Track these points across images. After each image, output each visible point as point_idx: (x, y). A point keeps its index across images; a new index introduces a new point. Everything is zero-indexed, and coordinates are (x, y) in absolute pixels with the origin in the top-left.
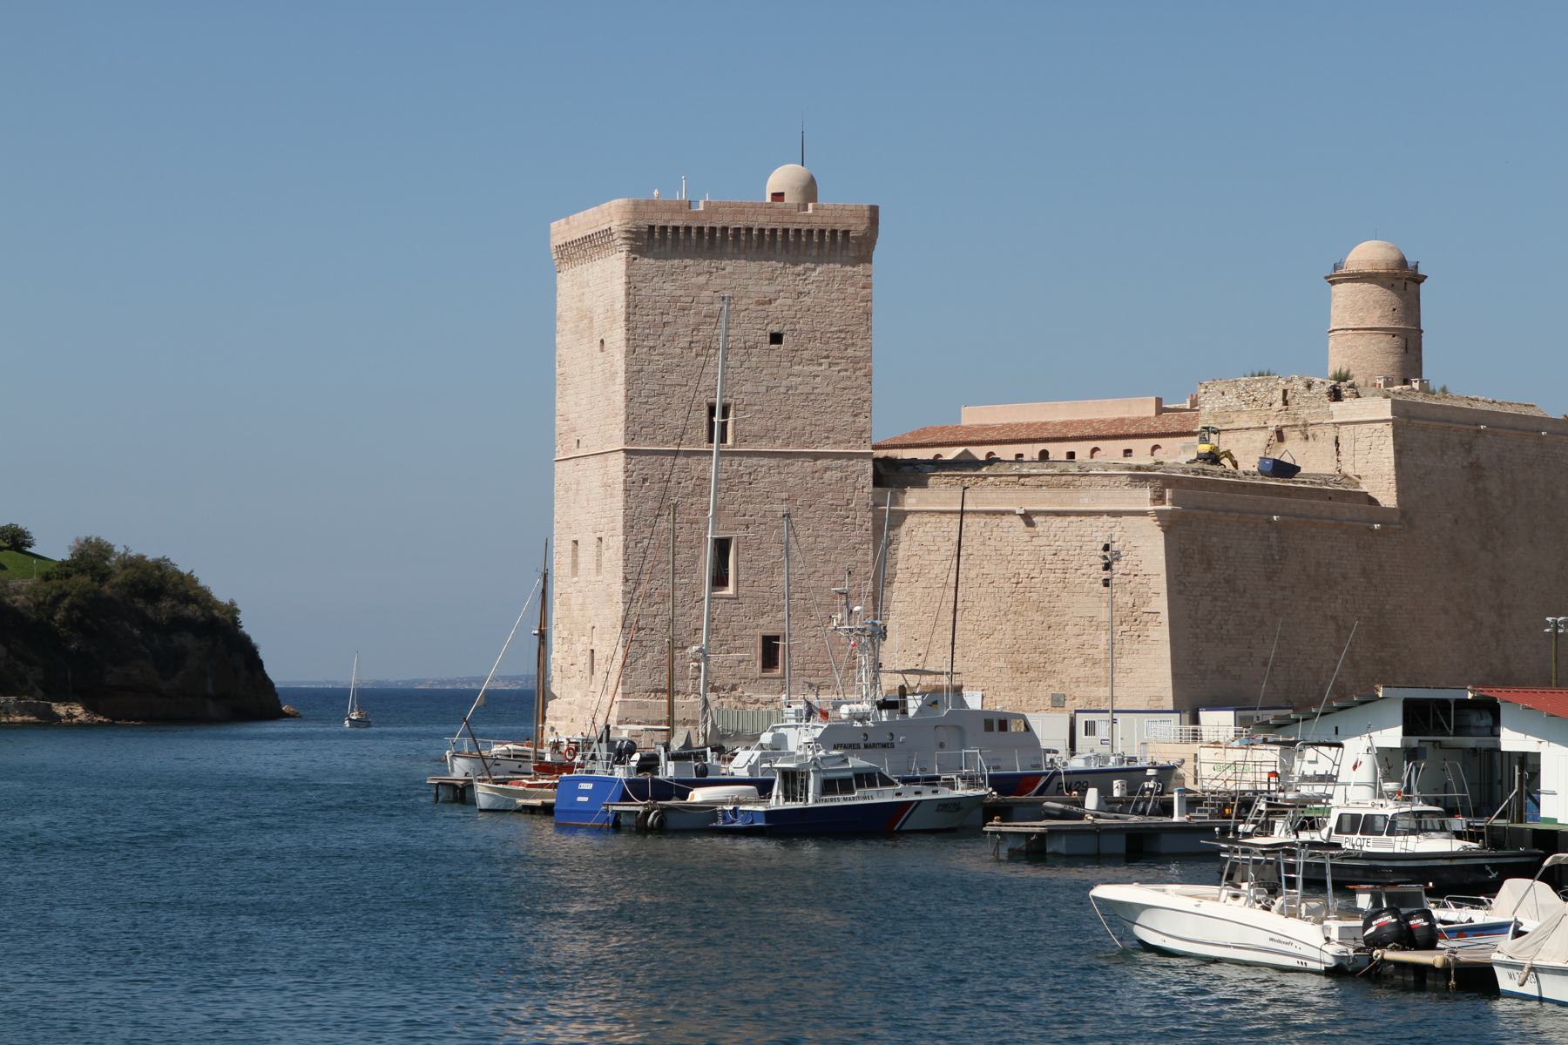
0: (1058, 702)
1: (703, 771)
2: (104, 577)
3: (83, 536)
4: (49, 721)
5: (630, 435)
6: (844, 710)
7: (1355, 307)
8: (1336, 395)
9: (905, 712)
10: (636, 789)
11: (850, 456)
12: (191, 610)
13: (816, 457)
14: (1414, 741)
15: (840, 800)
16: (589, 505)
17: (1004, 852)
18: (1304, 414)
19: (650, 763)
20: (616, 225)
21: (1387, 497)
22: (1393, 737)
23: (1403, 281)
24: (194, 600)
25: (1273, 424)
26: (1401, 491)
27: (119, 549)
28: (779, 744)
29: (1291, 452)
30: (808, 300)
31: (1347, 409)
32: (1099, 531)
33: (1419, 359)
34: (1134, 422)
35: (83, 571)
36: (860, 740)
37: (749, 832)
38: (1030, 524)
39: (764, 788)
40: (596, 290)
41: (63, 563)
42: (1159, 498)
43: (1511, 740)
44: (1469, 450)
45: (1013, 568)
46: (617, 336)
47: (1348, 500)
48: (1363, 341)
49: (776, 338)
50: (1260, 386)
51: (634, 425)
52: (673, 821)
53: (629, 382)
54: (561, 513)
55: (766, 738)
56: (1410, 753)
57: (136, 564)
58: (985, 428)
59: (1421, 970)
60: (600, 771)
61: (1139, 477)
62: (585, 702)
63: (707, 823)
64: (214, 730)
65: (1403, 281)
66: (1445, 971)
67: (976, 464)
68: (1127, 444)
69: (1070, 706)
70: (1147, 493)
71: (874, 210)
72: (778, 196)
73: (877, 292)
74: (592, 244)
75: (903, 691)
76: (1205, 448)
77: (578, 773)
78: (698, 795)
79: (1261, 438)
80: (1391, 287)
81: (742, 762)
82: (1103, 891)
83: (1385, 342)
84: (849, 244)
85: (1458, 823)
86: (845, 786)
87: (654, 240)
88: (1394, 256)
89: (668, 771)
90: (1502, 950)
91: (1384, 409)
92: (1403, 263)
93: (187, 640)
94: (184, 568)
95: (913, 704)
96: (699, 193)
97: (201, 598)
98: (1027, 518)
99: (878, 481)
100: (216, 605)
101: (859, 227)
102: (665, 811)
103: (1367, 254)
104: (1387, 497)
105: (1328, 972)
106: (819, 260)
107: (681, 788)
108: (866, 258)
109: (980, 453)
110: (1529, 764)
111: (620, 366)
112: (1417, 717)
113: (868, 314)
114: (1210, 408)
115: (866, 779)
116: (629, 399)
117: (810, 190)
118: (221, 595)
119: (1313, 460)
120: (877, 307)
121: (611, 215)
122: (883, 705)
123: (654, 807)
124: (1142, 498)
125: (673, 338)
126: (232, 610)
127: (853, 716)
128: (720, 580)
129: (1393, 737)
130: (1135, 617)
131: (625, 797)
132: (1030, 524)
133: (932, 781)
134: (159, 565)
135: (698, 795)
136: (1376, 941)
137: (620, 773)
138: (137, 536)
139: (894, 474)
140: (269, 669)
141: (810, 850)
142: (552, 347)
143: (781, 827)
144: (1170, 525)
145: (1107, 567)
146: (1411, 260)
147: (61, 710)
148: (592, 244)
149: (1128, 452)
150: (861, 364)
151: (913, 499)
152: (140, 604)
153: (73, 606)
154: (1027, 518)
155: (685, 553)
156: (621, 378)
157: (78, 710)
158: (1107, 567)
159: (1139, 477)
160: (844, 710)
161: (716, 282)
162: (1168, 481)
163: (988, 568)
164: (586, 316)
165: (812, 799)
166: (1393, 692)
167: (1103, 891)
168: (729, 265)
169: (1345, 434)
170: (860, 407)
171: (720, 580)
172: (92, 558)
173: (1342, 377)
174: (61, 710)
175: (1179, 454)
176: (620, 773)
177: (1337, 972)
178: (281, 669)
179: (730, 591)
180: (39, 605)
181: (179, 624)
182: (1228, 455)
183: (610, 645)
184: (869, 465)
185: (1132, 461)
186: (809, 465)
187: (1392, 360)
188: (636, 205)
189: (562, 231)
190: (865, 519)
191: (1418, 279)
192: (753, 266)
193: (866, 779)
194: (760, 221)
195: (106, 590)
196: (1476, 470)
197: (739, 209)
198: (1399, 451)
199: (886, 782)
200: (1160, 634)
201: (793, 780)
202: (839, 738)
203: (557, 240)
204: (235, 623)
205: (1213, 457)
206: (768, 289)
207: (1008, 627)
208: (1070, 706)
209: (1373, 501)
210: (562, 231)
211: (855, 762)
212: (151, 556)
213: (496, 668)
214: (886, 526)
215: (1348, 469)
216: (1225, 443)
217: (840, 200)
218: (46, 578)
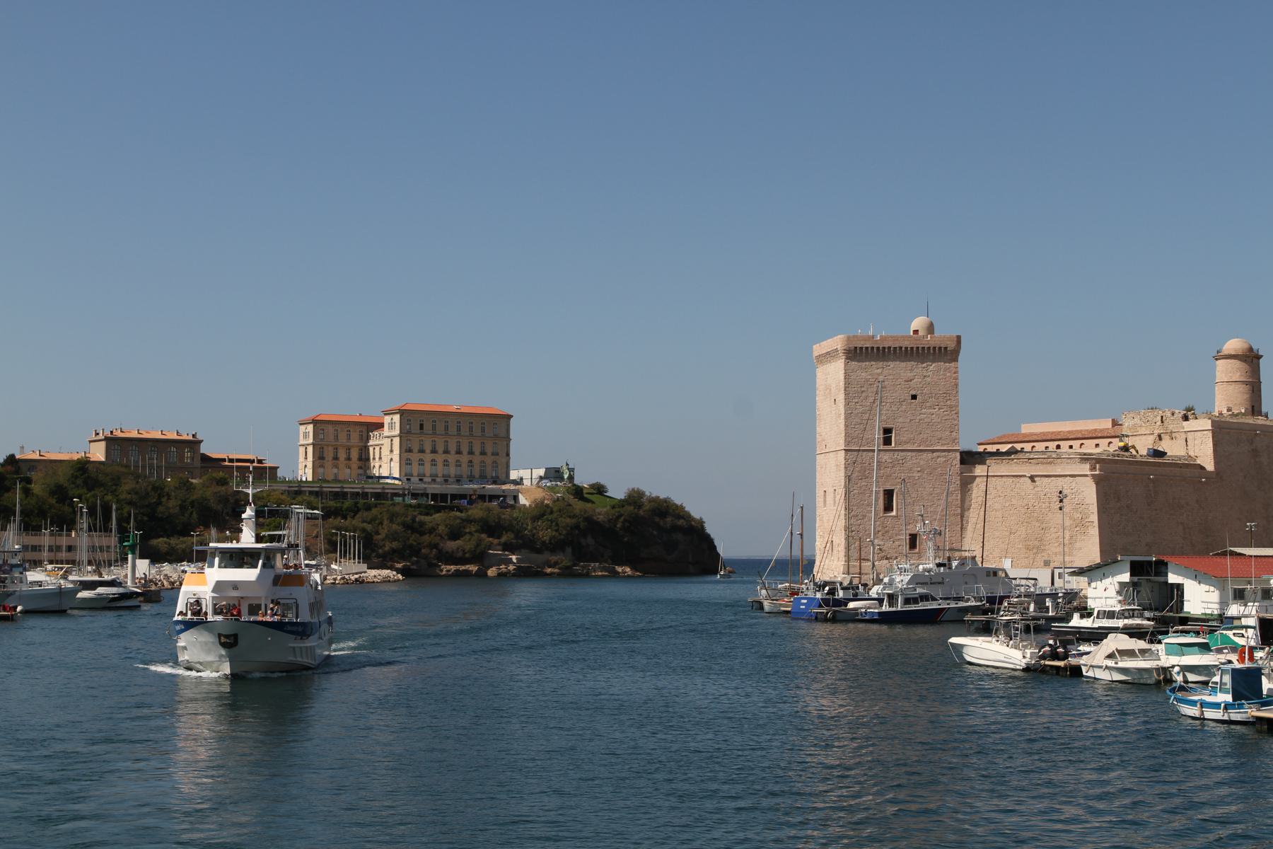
0: (1047, 563)
1: (856, 595)
2: (640, 507)
3: (631, 487)
4: (614, 575)
5: (847, 442)
6: (921, 567)
7: (1227, 371)
8: (1186, 418)
9: (950, 568)
10: (826, 602)
11: (949, 451)
12: (681, 522)
13: (933, 451)
14: (1136, 579)
15: (913, 607)
16: (830, 473)
17: (972, 628)
18: (1171, 427)
19: (832, 592)
20: (839, 347)
21: (1210, 467)
22: (1126, 577)
23: (1251, 358)
24: (683, 518)
25: (1157, 432)
26: (1216, 463)
27: (647, 494)
28: (891, 582)
29: (1165, 446)
30: (928, 379)
31: (1191, 425)
32: (1052, 486)
33: (1260, 396)
34: (1101, 430)
35: (630, 504)
36: (928, 580)
37: (872, 621)
38: (1033, 481)
39: (881, 601)
40: (832, 375)
41: (621, 500)
42: (1093, 468)
43: (1173, 578)
44: (1252, 443)
45: (1026, 502)
46: (841, 398)
47: (1190, 469)
48: (1232, 387)
49: (914, 397)
50: (1150, 415)
51: (849, 438)
52: (839, 616)
53: (846, 418)
54: (819, 478)
55: (886, 580)
56: (1134, 585)
57: (655, 500)
58: (1032, 434)
59: (1058, 668)
60: (810, 594)
61: (1085, 458)
62: (831, 566)
63: (854, 617)
64: (695, 579)
65: (1251, 358)
66: (1065, 668)
67: (1016, 452)
68: (1097, 441)
69: (1052, 565)
70: (1088, 466)
71: (959, 338)
72: (916, 332)
73: (960, 375)
74: (829, 356)
75: (949, 559)
76: (1122, 444)
77: (801, 595)
78: (851, 605)
79: (1151, 439)
80: (1245, 361)
81: (875, 591)
82: (954, 640)
83: (1242, 388)
84: (947, 353)
85: (1147, 614)
86: (915, 601)
87: (857, 353)
88: (1246, 346)
89: (841, 594)
90: (1082, 661)
91: (1208, 424)
92: (1251, 349)
93: (678, 537)
94: (678, 502)
95: (955, 564)
96: (877, 331)
97: (686, 516)
98: (1032, 478)
99: (962, 462)
100: (694, 519)
101: (951, 346)
102: (835, 612)
103: (1233, 345)
104: (1210, 467)
105: (1024, 670)
106: (933, 361)
107: (844, 602)
108: (956, 360)
109: (1018, 446)
110: (1180, 587)
111: (842, 411)
112: (1136, 569)
113: (957, 385)
114: (1128, 423)
115: (925, 598)
116: (846, 426)
117: (930, 328)
118: (696, 514)
119: (1174, 449)
120: (960, 382)
121: (837, 342)
122: (939, 565)
123: (833, 608)
124: (1085, 468)
125: (866, 397)
126: (701, 522)
127: (925, 570)
128: (888, 508)
129: (1126, 577)
130: (1082, 524)
131: (820, 606)
132: (1033, 481)
133: (959, 599)
134: (666, 501)
135: (851, 605)
136: (1043, 657)
137: (819, 595)
138: (656, 489)
139: (970, 459)
140: (720, 550)
141: (899, 630)
142: (815, 402)
143: (885, 618)
144: (1098, 481)
145: (1061, 501)
146: (1255, 348)
147: (619, 569)
148: (829, 356)
149: (1097, 445)
150: (954, 408)
151: (979, 470)
152: (657, 519)
153: (625, 520)
154: (1032, 478)
155: (875, 498)
156: (843, 417)
157: (628, 569)
158: (1061, 501)
159: (1085, 458)
160: (921, 567)
161: (886, 372)
162: (1099, 461)
163: (1014, 502)
164: (828, 388)
165: (899, 607)
166: (1125, 558)
167: (954, 640)
168: (892, 364)
169: (1190, 436)
170: (953, 428)
171: (888, 508)
172: (635, 498)
173: (1189, 410)
174: (619, 569)
175: (1108, 448)
176: (819, 595)
177: (1027, 669)
178: (725, 549)
179: (894, 513)
180: (610, 520)
181: (675, 528)
182: (1133, 447)
183: (840, 539)
184: (958, 455)
185: (1084, 450)
186: (930, 455)
187: (1246, 396)
188: (849, 338)
189: (818, 349)
190: (956, 480)
191: (1259, 357)
192: (903, 364)
193: (925, 598)
194: (906, 344)
195: (641, 512)
196: (1255, 453)
197: (895, 339)
198: (1215, 445)
199: (934, 599)
200: (1094, 531)
201: (892, 598)
202: (917, 580)
203: (816, 354)
204: (703, 528)
205: (1126, 449)
206: (910, 375)
207: (1023, 529)
208: (1052, 565)
209: (1202, 468)
210: (818, 349)
211: (919, 590)
212: (662, 496)
213: (778, 550)
214: (966, 483)
215: (1191, 453)
216: (1130, 442)
217: (944, 333)
218: (613, 507)
